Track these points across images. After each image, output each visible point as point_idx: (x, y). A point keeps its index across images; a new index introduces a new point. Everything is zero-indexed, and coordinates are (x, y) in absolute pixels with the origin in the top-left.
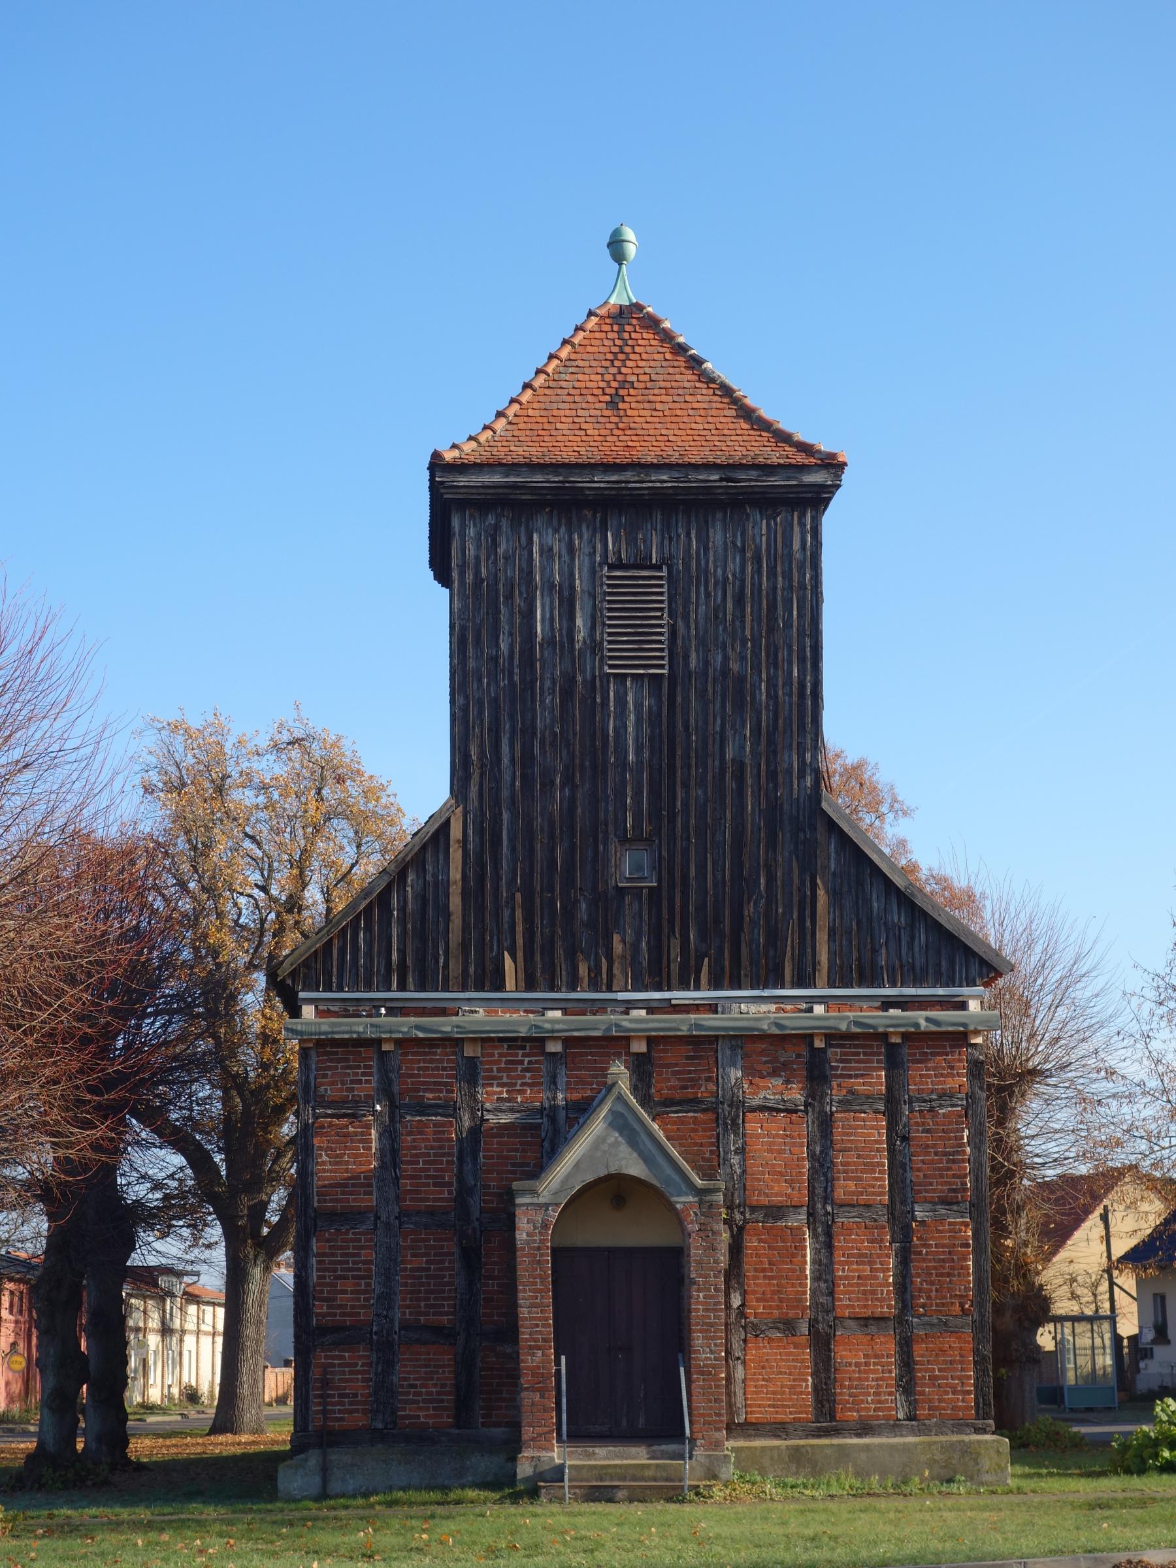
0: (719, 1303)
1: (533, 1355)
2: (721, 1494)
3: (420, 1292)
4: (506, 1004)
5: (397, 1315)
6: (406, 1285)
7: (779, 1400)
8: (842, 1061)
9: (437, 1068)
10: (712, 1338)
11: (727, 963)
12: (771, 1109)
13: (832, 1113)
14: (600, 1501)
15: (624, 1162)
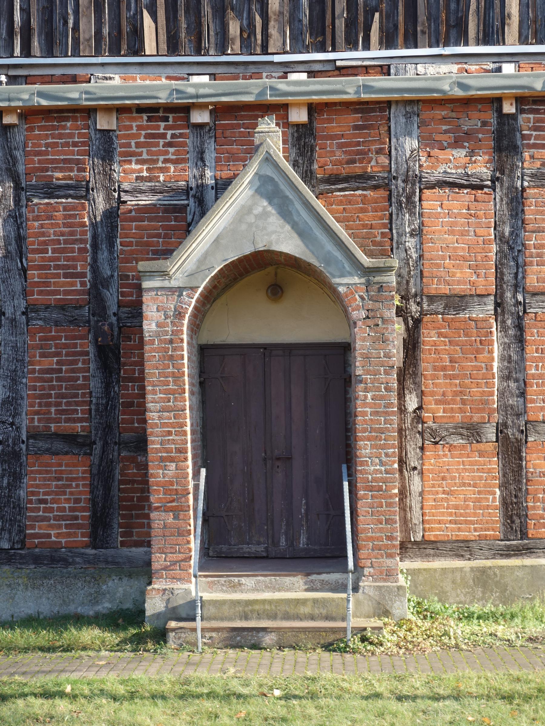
0: (390, 405)
1: (165, 468)
2: (395, 638)
3: (50, 396)
4: (150, 69)
5: (24, 422)
6: (34, 388)
7: (461, 515)
8: (536, 129)
9: (67, 144)
10: (383, 447)
11: (401, 18)
12: (452, 185)
13: (523, 189)
14: (242, 647)
15: (274, 237)
